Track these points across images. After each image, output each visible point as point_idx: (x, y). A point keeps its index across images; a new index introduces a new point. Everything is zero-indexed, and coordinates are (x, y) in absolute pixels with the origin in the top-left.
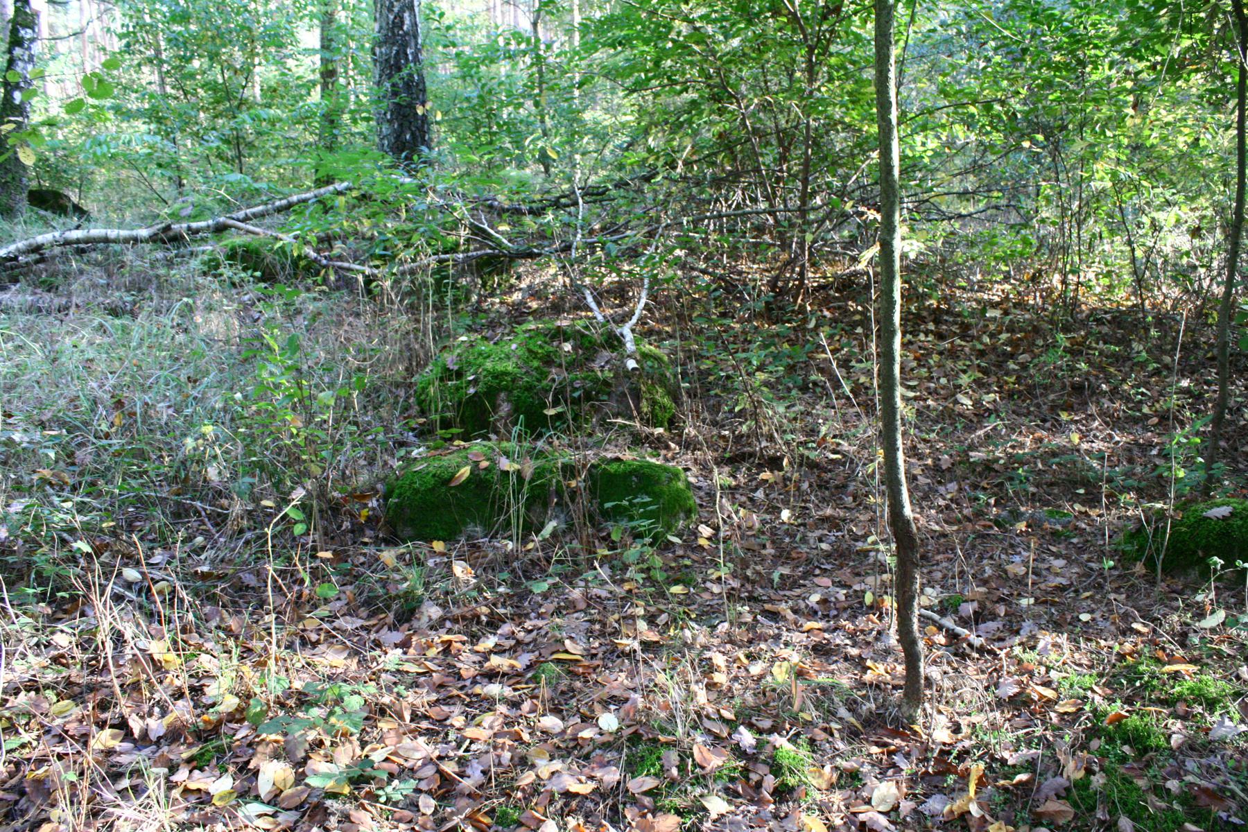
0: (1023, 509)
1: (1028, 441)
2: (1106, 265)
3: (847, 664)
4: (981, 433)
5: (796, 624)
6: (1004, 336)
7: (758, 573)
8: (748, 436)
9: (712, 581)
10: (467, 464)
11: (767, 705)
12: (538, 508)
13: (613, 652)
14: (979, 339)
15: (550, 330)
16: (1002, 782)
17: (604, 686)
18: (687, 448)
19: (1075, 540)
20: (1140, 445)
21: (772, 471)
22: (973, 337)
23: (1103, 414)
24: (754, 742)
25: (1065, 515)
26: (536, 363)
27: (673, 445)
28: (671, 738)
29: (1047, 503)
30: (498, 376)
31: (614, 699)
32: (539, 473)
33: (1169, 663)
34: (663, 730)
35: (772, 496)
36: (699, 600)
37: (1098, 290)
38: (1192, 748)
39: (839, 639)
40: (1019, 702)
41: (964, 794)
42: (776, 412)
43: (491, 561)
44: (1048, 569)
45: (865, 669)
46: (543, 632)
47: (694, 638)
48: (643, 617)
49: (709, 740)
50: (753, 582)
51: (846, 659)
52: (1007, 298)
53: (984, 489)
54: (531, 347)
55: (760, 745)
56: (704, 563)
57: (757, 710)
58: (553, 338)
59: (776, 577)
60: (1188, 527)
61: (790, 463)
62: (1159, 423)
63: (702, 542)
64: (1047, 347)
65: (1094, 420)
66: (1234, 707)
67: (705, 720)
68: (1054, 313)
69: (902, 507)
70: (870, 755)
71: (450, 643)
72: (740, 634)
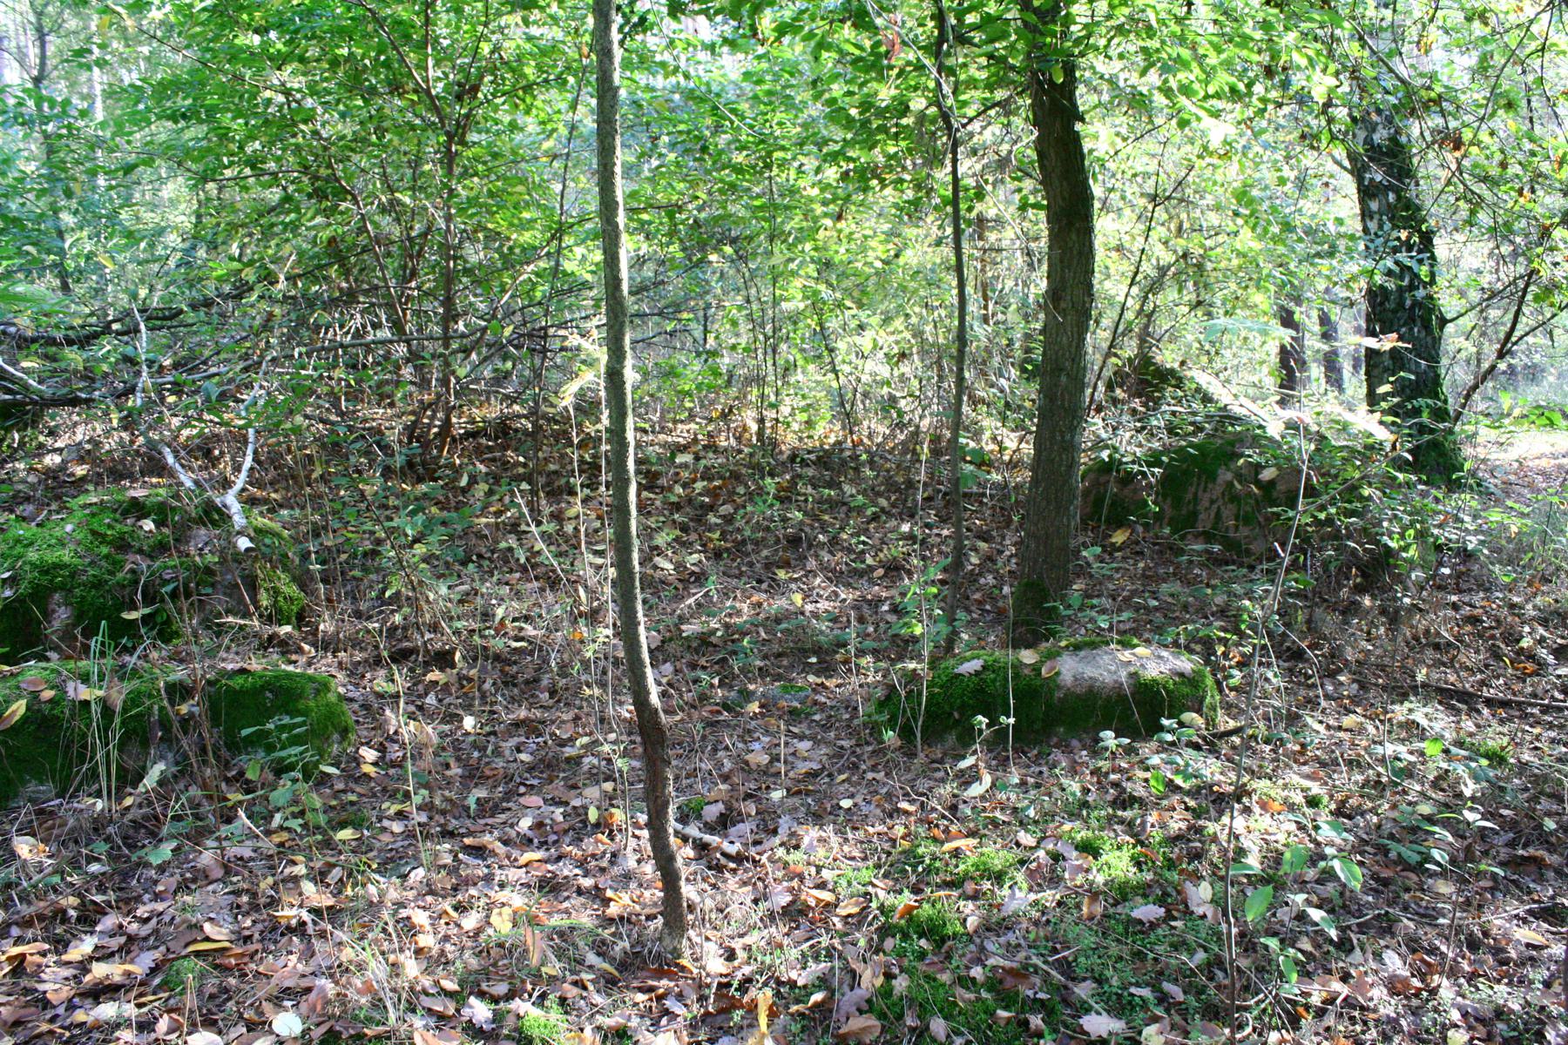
0: (752, 687)
1: (745, 607)
2: (804, 397)
3: (582, 900)
4: (691, 601)
5: (508, 857)
6: (699, 485)
7: (450, 801)
8: (405, 628)
9: (390, 819)
10: (19, 697)
11: (495, 965)
12: (135, 748)
13: (274, 929)
14: (670, 489)
15: (120, 503)
16: (794, 1008)
17: (268, 977)
18: (325, 649)
19: (817, 717)
20: (869, 602)
21: (442, 670)
22: (663, 488)
23: (824, 568)
24: (490, 1015)
25: (801, 689)
26: (105, 550)
27: (306, 647)
28: (381, 1028)
29: (778, 677)
30: (47, 570)
31: (287, 992)
32: (133, 700)
33: (948, 840)
34: (369, 1020)
35: (446, 701)
36: (378, 845)
37: (795, 427)
38: (988, 929)
39: (566, 870)
40: (794, 913)
41: (755, 1031)
42: (440, 593)
43: (73, 830)
44: (794, 754)
45: (607, 902)
46: (167, 918)
47: (382, 894)
48: (307, 876)
49: (432, 1022)
50: (443, 813)
51: (580, 892)
52: (695, 440)
53: (704, 668)
54: (95, 527)
55: (498, 1017)
56: (374, 795)
57: (485, 973)
58: (125, 514)
59: (471, 802)
60: (941, 687)
61: (464, 657)
62: (885, 575)
63: (367, 769)
64: (750, 496)
65: (815, 576)
66: (1020, 877)
67: (422, 997)
68: (751, 455)
69: (648, 693)
70: (636, 1004)
71: (22, 956)
72: (442, 880)
